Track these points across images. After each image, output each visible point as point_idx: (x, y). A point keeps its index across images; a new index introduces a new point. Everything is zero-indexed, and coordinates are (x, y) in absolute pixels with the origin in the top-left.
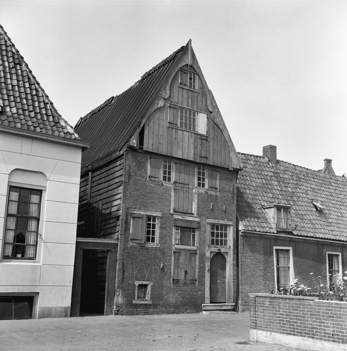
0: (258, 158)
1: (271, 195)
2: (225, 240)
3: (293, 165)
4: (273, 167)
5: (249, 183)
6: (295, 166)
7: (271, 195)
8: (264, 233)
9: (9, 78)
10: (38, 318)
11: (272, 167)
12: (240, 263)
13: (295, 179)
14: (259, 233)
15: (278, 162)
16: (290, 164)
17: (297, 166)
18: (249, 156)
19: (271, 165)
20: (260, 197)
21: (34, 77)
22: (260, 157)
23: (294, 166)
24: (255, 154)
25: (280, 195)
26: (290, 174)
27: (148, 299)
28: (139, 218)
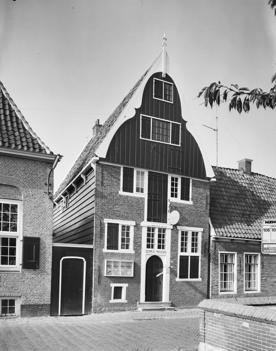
0: (234, 170)
1: (244, 204)
2: (196, 243)
3: (267, 177)
4: (247, 178)
5: (237, 191)
6: (269, 178)
7: (244, 204)
8: (251, 240)
9: (3, 119)
10: (53, 247)
11: (247, 179)
12: (91, 221)
13: (268, 189)
14: (229, 238)
15: (253, 174)
16: (264, 176)
17: (271, 178)
18: (225, 170)
19: (245, 177)
20: (233, 206)
21: (7, 94)
22: (236, 170)
23: (268, 178)
24: (231, 168)
25: (252, 204)
26: (264, 185)
27: (123, 299)
28: (263, 264)
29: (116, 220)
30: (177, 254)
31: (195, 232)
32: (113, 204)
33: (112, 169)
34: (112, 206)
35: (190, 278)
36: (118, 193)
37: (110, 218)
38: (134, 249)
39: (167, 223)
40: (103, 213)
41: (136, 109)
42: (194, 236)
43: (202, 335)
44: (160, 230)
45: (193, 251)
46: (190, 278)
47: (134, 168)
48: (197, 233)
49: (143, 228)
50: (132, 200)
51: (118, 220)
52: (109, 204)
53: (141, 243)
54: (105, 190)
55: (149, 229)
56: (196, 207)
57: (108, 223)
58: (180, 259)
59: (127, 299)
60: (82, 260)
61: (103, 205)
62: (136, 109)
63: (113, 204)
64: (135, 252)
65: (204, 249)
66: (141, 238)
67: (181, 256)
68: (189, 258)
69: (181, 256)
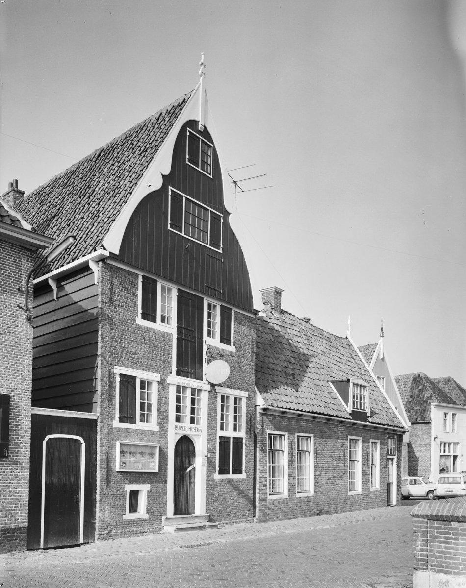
30: (216, 434)
35: (233, 473)
36: (135, 321)
38: (159, 423)
41: (163, 176)
42: (145, 411)
44: (193, 390)
45: (235, 429)
46: (233, 473)
55: (179, 389)
56: (239, 357)
60: (79, 441)
61: (113, 340)
62: (163, 176)
64: (160, 428)
66: (167, 403)
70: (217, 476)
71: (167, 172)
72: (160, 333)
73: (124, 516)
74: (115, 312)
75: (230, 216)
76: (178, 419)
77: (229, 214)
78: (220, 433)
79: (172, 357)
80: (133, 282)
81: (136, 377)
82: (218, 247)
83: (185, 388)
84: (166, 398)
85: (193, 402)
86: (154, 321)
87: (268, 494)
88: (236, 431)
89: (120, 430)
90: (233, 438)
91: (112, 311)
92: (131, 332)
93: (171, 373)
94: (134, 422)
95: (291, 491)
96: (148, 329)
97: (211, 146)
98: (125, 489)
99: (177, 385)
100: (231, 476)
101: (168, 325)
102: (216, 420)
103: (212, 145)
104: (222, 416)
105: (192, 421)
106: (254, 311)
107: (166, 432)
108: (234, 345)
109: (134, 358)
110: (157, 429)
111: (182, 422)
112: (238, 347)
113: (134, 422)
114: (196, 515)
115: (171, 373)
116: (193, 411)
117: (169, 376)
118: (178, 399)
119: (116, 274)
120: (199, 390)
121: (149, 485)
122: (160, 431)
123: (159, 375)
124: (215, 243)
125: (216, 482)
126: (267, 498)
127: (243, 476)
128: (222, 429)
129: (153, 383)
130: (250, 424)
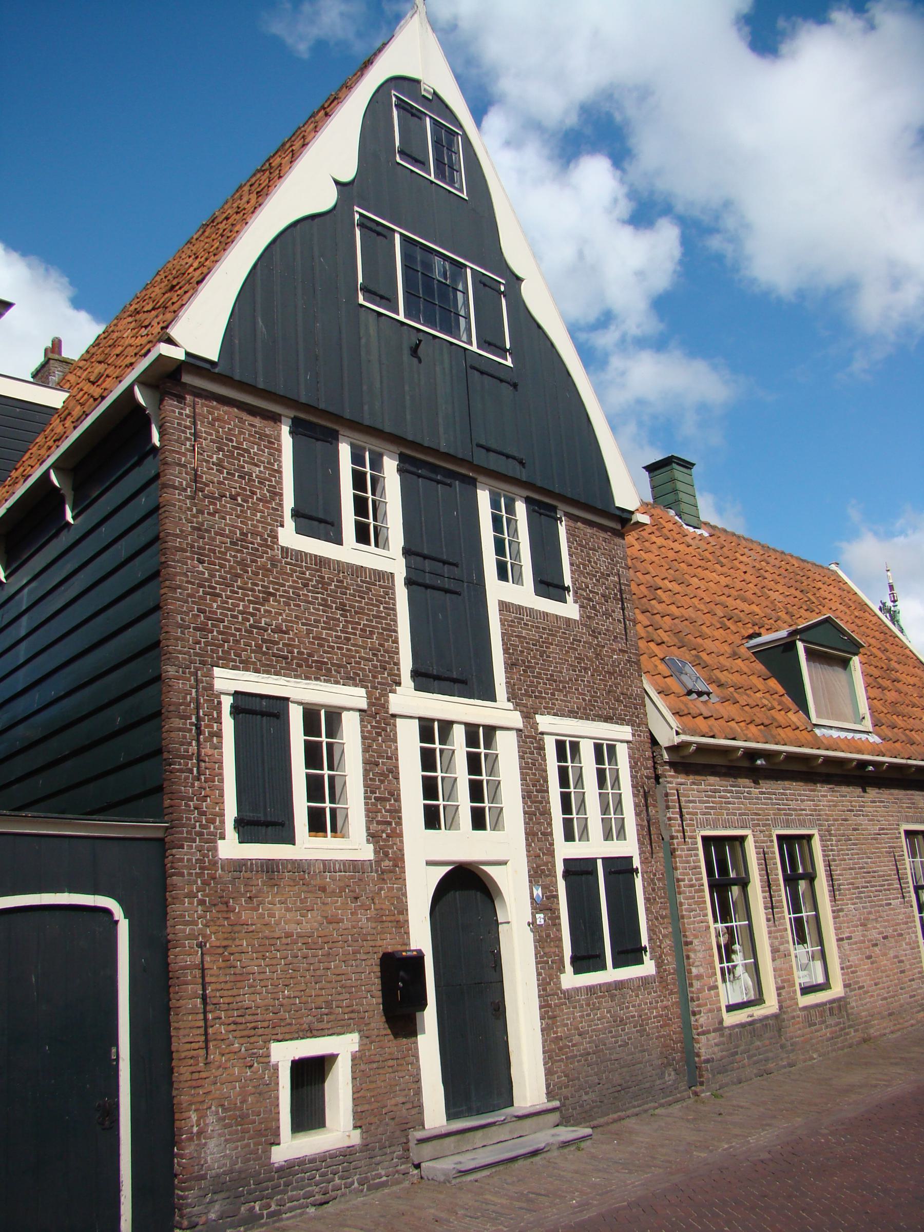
28: (831, 875)
29: (273, 679)
30: (551, 853)
31: (568, 739)
32: (253, 590)
33: (241, 420)
34: (250, 602)
35: (615, 966)
36: (276, 537)
37: (246, 665)
38: (373, 837)
39: (495, 701)
40: (206, 637)
41: (337, 183)
42: (322, 769)
43: (673, 795)
44: (472, 733)
45: (608, 836)
46: (615, 966)
47: (341, 432)
48: (334, 716)
49: (399, 721)
50: (342, 582)
51: (282, 680)
52: (233, 592)
53: (398, 800)
54: (212, 515)
55: (426, 729)
56: (594, 633)
57: (237, 694)
58: (567, 874)
59: (360, 1127)
60: (107, 912)
61: (205, 593)
62: (337, 183)
63: (253, 590)
64: (376, 852)
65: (645, 823)
66: (394, 772)
67: (566, 861)
68: (600, 863)
69: (566, 861)
70: (570, 980)
71: (348, 173)
72: (358, 571)
73: (274, 1149)
74: (212, 515)
75: (524, 286)
76: (432, 819)
77: (519, 280)
78: (564, 850)
79: (397, 638)
80: (267, 436)
81: (287, 699)
82: (501, 350)
83: (447, 726)
84: (389, 758)
85: (474, 764)
86: (339, 541)
87: (724, 1009)
88: (573, 839)
89: (240, 865)
90: (604, 859)
91: (200, 512)
92: (263, 567)
93: (399, 684)
94: (291, 840)
95: (783, 992)
96: (322, 562)
97: (458, 134)
98: (274, 1059)
99: (421, 719)
100: (611, 974)
101: (379, 551)
102: (547, 813)
103: (461, 133)
104: (566, 800)
105: (478, 821)
106: (618, 513)
107: (398, 861)
108: (576, 602)
109: (277, 643)
110: (367, 853)
111: (494, 829)
112: (584, 601)
113: (291, 840)
114: (520, 1113)
115: (399, 684)
116: (476, 791)
117: (394, 692)
118: (428, 760)
119: (212, 414)
120: (491, 730)
121: (355, 1037)
122: (378, 862)
123: (362, 692)
124: (491, 342)
125: (570, 995)
126: (721, 1022)
127: (647, 968)
128: (569, 836)
129: (345, 715)
130: (648, 815)
